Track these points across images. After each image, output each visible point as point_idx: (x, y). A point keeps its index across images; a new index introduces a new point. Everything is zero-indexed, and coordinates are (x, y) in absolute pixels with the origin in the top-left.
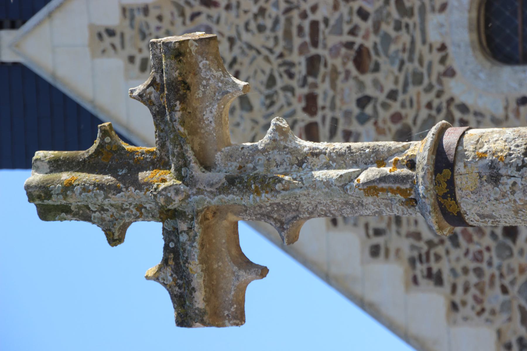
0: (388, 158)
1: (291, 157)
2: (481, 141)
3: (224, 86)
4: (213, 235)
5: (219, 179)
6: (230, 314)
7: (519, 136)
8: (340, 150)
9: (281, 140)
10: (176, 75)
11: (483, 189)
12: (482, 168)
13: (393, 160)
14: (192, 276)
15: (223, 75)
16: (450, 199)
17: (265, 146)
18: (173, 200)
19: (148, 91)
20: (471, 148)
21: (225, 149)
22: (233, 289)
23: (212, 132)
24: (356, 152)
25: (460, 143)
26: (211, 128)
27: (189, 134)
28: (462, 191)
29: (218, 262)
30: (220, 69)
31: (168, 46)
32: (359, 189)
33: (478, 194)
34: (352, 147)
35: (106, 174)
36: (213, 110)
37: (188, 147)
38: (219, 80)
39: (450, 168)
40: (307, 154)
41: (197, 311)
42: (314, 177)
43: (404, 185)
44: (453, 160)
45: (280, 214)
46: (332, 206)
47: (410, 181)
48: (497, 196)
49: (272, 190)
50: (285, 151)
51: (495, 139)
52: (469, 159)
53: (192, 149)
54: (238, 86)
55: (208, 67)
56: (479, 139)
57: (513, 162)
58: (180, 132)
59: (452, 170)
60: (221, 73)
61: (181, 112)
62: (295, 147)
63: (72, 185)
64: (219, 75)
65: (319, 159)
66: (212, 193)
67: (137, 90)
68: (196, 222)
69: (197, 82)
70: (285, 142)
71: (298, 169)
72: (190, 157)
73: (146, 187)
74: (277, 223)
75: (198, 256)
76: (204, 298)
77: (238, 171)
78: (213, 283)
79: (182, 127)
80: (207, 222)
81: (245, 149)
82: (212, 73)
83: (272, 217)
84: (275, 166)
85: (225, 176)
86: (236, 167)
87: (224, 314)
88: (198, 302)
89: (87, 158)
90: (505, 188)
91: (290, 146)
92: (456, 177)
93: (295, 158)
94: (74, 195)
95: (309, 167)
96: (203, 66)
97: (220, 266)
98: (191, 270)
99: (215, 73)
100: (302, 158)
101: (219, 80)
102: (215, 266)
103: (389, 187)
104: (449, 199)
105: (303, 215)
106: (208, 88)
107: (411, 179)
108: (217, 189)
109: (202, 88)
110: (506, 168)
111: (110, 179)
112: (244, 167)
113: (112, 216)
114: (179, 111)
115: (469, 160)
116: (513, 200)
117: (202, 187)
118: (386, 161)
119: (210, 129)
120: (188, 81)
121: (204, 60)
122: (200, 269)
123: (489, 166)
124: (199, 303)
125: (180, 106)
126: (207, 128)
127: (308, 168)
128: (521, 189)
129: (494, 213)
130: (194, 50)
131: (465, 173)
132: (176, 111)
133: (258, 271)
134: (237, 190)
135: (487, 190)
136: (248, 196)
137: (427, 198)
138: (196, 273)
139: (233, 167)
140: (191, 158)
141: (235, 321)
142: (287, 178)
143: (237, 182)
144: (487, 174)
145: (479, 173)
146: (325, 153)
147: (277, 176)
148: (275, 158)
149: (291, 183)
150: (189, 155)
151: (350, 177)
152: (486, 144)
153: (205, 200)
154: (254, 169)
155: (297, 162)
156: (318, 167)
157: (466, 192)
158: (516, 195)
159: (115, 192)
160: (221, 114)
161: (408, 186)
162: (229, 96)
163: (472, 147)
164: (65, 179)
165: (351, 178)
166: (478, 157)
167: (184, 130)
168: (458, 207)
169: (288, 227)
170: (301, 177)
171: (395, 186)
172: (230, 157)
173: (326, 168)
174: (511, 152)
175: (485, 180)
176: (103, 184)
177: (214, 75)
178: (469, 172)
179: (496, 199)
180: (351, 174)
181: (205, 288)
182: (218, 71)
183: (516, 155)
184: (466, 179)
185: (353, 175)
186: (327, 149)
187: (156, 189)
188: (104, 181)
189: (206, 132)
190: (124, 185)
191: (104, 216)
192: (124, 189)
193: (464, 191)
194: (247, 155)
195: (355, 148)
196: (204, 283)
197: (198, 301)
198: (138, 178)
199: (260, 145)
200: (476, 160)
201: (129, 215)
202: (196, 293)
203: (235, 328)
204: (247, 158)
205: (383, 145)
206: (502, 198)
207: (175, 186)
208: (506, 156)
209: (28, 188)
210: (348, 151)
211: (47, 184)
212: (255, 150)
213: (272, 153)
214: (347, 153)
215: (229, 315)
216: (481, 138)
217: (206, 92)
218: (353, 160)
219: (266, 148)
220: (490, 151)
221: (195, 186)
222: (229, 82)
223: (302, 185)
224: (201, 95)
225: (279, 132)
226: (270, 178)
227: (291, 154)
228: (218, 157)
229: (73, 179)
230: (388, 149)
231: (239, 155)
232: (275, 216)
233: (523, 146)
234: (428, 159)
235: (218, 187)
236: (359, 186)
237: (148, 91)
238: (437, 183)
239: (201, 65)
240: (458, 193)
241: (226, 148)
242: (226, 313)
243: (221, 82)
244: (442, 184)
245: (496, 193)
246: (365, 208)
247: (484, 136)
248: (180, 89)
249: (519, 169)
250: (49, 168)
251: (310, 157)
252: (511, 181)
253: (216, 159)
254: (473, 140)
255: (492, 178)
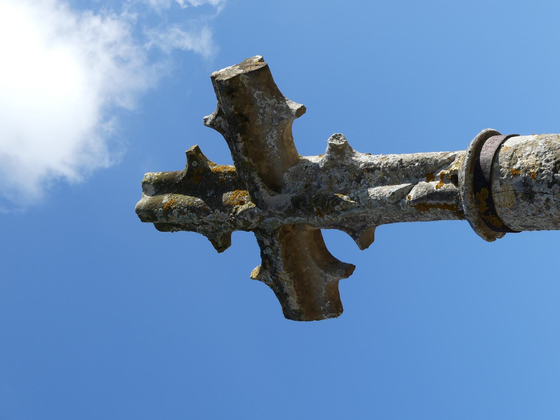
0: (436, 170)
1: (349, 173)
2: (515, 155)
3: (279, 114)
4: (296, 245)
5: (285, 202)
6: (326, 309)
7: (550, 148)
8: (392, 164)
9: (338, 159)
10: (232, 110)
11: (520, 205)
12: (516, 185)
13: (439, 174)
14: (283, 283)
15: (277, 102)
16: (492, 215)
17: (325, 165)
18: (250, 223)
19: (217, 120)
20: (505, 164)
21: (292, 169)
22: (323, 288)
23: (277, 155)
24: (407, 166)
25: (496, 159)
26: (275, 152)
27: (254, 162)
28: (501, 208)
29: (306, 267)
30: (274, 96)
31: (220, 84)
32: (410, 206)
33: (516, 210)
34: (403, 160)
35: (197, 196)
36: (274, 136)
37: (255, 175)
38: (273, 107)
39: (487, 187)
40: (363, 170)
41: (293, 313)
42: (369, 195)
43: (450, 202)
44: (489, 179)
45: (350, 224)
46: (394, 216)
47: (454, 197)
48: (534, 212)
49: (332, 212)
50: (344, 168)
51: (528, 153)
52: (504, 176)
53: (260, 175)
54: (291, 112)
55: (262, 97)
56: (513, 153)
57: (544, 178)
58: (245, 161)
59: (490, 189)
60: (275, 100)
61: (243, 143)
62: (352, 164)
63: (171, 208)
64: (274, 102)
65: (374, 174)
66: (282, 216)
67: (209, 119)
68: (275, 239)
69: (255, 111)
70: (341, 161)
71: (357, 185)
72: (258, 183)
73: (229, 209)
74: (349, 232)
75: (283, 268)
76: (297, 301)
77: (305, 189)
78: (305, 284)
79: (246, 157)
80: (288, 234)
81: (308, 168)
82: (266, 102)
83: (344, 227)
84: (336, 183)
85: (291, 198)
86: (302, 185)
87: (321, 309)
88: (293, 305)
89: (182, 180)
90: (539, 204)
91: (347, 164)
92: (494, 195)
93: (353, 175)
94: (173, 217)
95: (367, 183)
96: (257, 96)
97: (309, 270)
98: (281, 279)
99: (269, 101)
100: (359, 174)
101: (273, 107)
102: (305, 270)
103: (436, 203)
104: (491, 216)
105: (370, 224)
106: (265, 115)
107: (456, 195)
108: (285, 212)
109: (260, 116)
110: (538, 186)
111: (200, 201)
112: (310, 185)
113: (213, 228)
114: (241, 142)
115: (504, 178)
116: (548, 214)
117: (272, 210)
118: (434, 174)
119: (274, 153)
120: (245, 112)
121: (257, 91)
122: (288, 277)
123: (522, 183)
124: (294, 306)
125: (241, 137)
126: (271, 152)
127: (365, 184)
128: (555, 205)
129: (535, 225)
130: (247, 83)
131: (502, 191)
132: (239, 142)
133: (342, 271)
134: (302, 213)
135: (524, 206)
136: (313, 217)
137: (470, 216)
138: (286, 281)
139: (301, 186)
140: (258, 184)
141: (331, 314)
142: (345, 197)
143: (301, 205)
144: (521, 191)
145: (514, 190)
146: (379, 169)
147: (337, 196)
148: (335, 175)
149: (348, 204)
150: (257, 182)
151: (402, 193)
152: (519, 159)
153: (277, 222)
154: (319, 187)
155: (355, 179)
156: (375, 182)
157: (505, 209)
158: (551, 210)
159: (205, 214)
160: (282, 138)
161: (454, 202)
162: (285, 121)
163: (506, 163)
164: (166, 202)
165: (403, 193)
166: (512, 175)
167: (248, 159)
168: (501, 222)
169: (359, 236)
170: (357, 196)
171: (442, 203)
172: (295, 176)
173: (381, 184)
174: (542, 168)
175: (521, 197)
176: (194, 207)
177: (268, 104)
178: (505, 190)
179: (534, 215)
180: (403, 190)
181: (297, 292)
182: (272, 99)
183: (546, 172)
184: (503, 197)
185: (405, 191)
186: (380, 164)
187: (235, 213)
188: (195, 204)
189: (271, 155)
190: (211, 208)
191: (206, 228)
192: (211, 212)
193: (503, 208)
194: (311, 174)
195: (405, 162)
196: (294, 288)
197: (292, 304)
198: (222, 200)
199: (321, 164)
200: (510, 177)
201: (226, 227)
202: (289, 297)
203: (332, 319)
204: (311, 177)
205: (430, 158)
206: (539, 213)
207: (250, 210)
208: (537, 173)
209: (138, 212)
210: (400, 165)
211: (152, 208)
212: (317, 169)
213: (332, 170)
214: (399, 167)
215: (325, 310)
216: (515, 153)
217: (265, 119)
218: (405, 174)
219: (326, 167)
220: (523, 168)
221: (266, 209)
222: (284, 108)
223: (359, 205)
224: (260, 123)
225: (335, 152)
226: (329, 200)
227: (349, 171)
228: (285, 177)
229: (171, 202)
230: (435, 162)
231: (303, 174)
232: (347, 226)
233: (553, 162)
234: (466, 179)
235: (285, 210)
236: (410, 203)
237: (217, 120)
238: (477, 202)
239: (255, 96)
240: (498, 210)
241: (292, 168)
242: (322, 308)
243: (275, 110)
244: (482, 202)
245: (532, 209)
246: (424, 216)
247: (518, 149)
248: (239, 122)
249: (550, 185)
250: (155, 190)
251: (366, 173)
252: (544, 198)
253: (284, 179)
254: (507, 155)
255: (527, 196)
